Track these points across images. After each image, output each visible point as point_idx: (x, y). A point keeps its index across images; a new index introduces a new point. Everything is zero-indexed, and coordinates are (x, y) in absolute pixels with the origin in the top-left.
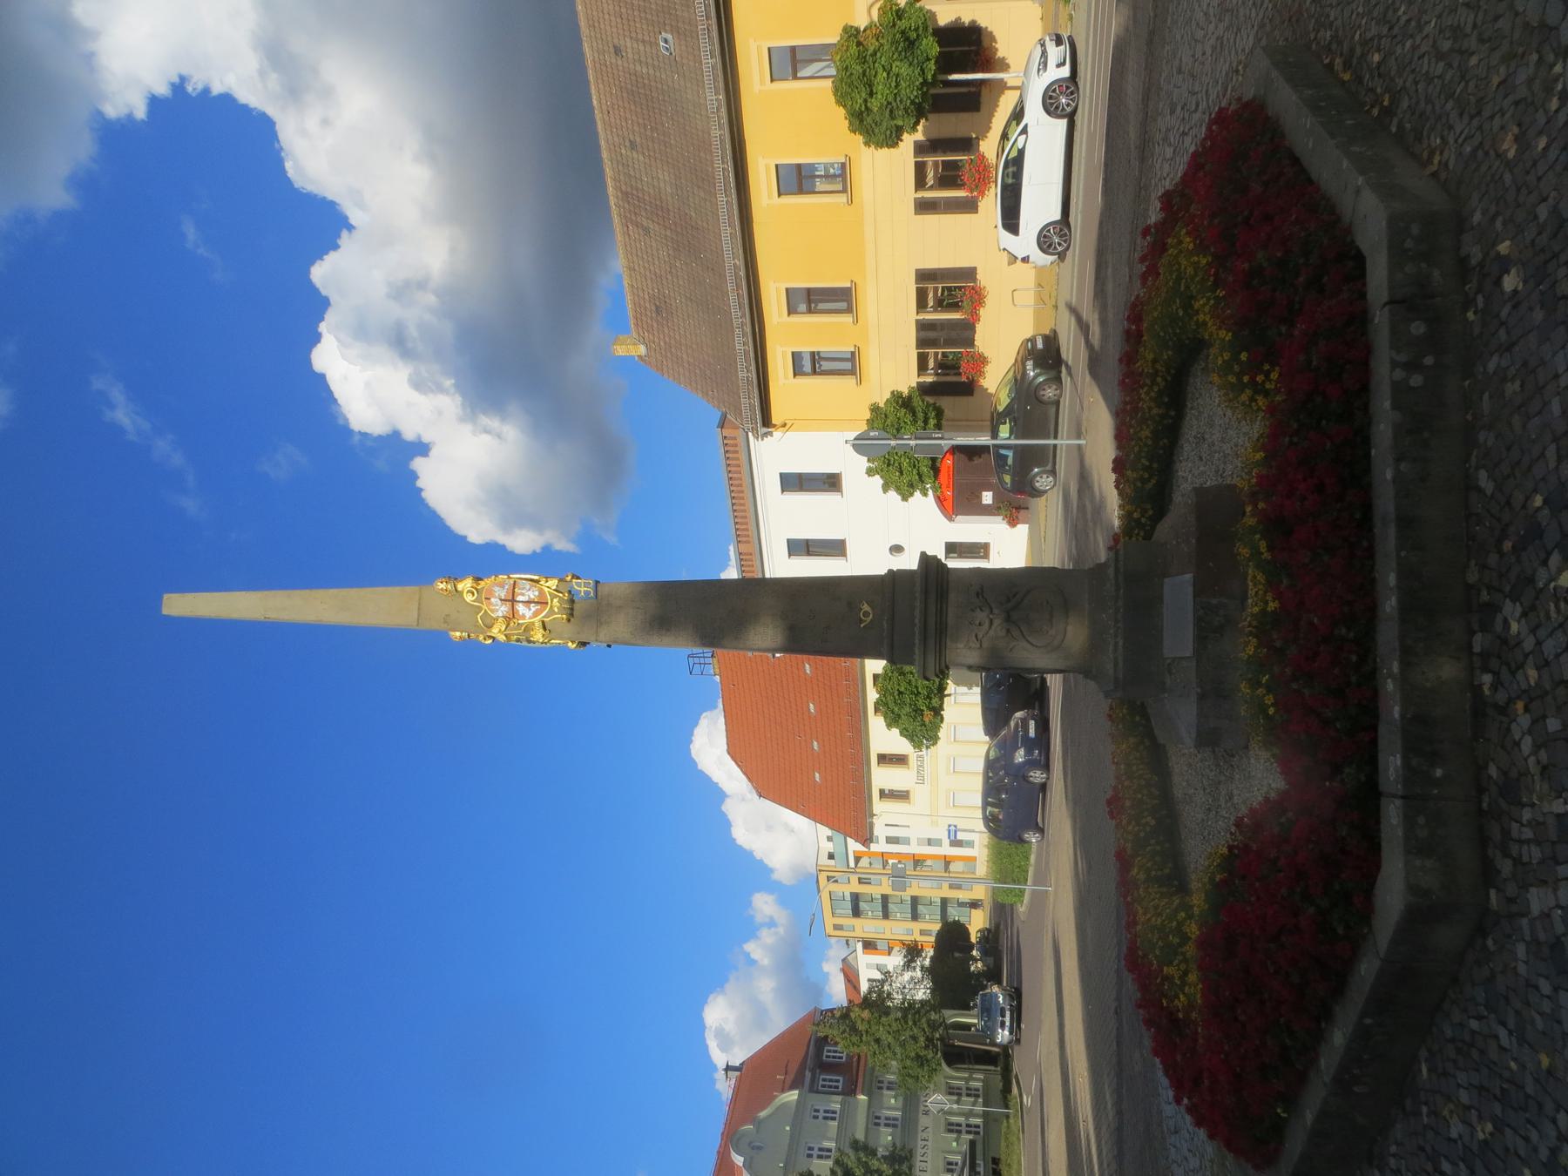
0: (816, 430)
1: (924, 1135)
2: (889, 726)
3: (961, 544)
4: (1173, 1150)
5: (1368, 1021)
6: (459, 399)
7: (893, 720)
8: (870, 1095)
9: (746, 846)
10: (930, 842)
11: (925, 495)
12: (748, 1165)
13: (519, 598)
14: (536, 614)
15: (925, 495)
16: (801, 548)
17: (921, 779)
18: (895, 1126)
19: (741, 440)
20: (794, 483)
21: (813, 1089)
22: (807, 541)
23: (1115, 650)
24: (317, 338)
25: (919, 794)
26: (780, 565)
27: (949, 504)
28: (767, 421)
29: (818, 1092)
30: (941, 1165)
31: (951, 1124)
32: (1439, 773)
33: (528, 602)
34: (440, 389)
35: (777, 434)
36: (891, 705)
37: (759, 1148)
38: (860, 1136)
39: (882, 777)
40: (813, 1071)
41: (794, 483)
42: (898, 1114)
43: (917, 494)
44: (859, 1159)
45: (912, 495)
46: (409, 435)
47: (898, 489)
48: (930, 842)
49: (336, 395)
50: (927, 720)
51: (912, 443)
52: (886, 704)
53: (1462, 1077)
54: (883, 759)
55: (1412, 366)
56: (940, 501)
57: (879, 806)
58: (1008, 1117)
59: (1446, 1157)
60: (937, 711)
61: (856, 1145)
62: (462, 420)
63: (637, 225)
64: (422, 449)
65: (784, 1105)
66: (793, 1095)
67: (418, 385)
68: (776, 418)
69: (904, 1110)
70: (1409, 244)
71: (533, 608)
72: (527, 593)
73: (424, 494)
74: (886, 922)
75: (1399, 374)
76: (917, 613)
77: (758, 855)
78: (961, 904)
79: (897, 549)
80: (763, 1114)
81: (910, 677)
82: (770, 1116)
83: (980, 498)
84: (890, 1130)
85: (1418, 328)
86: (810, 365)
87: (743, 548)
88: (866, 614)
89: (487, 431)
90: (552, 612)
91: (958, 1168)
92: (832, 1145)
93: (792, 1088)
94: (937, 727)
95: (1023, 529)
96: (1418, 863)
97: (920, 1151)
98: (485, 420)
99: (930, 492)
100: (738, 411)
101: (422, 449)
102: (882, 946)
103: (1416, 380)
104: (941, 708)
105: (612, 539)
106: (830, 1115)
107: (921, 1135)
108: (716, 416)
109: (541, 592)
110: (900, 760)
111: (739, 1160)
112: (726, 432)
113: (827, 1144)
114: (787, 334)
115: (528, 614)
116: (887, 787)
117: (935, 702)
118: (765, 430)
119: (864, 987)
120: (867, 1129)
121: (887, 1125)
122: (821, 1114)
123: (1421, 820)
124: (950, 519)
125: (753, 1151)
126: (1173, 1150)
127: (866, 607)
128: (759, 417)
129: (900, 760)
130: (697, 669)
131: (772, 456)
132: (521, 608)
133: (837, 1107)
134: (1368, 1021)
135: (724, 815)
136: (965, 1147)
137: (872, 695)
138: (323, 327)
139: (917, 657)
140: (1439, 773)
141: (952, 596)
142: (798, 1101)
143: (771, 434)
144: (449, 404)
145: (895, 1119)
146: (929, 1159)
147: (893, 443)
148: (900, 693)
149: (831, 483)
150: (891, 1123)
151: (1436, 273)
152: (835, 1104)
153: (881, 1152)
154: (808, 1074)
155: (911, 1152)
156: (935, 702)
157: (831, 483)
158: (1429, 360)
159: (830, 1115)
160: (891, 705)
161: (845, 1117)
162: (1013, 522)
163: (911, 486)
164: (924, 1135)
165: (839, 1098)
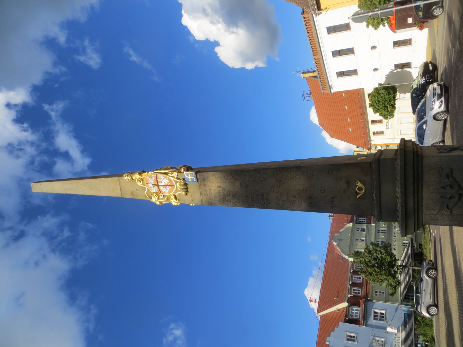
1: (395, 235)
2: (375, 113)
3: (399, 41)
6: (224, 24)
7: (376, 110)
8: (376, 223)
9: (331, 144)
11: (384, 26)
12: (338, 245)
13: (160, 184)
14: (170, 191)
15: (384, 26)
17: (388, 127)
18: (385, 233)
19: (311, 18)
20: (332, 30)
21: (357, 223)
22: (339, 51)
24: (182, 16)
27: (394, 26)
28: (319, 8)
29: (358, 223)
30: (401, 244)
33: (165, 186)
34: (219, 22)
35: (324, 12)
36: (375, 106)
37: (341, 240)
38: (373, 241)
39: (373, 128)
40: (356, 217)
41: (332, 30)
42: (386, 229)
43: (381, 26)
44: (373, 248)
45: (378, 27)
46: (212, 40)
47: (373, 26)
49: (192, 33)
50: (389, 109)
51: (379, 12)
52: (373, 106)
54: (373, 122)
56: (391, 27)
57: (372, 137)
58: (425, 233)
60: (393, 106)
61: (372, 244)
62: (226, 31)
64: (216, 44)
65: (348, 228)
66: (351, 225)
67: (212, 23)
68: (323, 7)
69: (388, 228)
71: (169, 188)
72: (164, 180)
73: (220, 58)
77: (334, 146)
80: (341, 230)
81: (382, 95)
82: (344, 231)
83: (407, 21)
84: (383, 234)
87: (316, 57)
88: (360, 189)
89: (233, 33)
90: (177, 190)
92: (364, 239)
93: (350, 222)
94: (393, 112)
95: (426, 30)
97: (393, 244)
98: (232, 29)
99: (386, 25)
100: (308, 6)
101: (216, 44)
104: (395, 104)
105: (277, 59)
106: (363, 230)
107: (393, 235)
108: (300, 10)
109: (170, 180)
110: (380, 121)
111: (335, 244)
112: (305, 16)
113: (362, 238)
115: (167, 191)
116: (375, 131)
117: (392, 103)
118: (319, 12)
120: (375, 234)
121: (382, 232)
122: (360, 230)
124: (395, 32)
125: (339, 241)
127: (359, 184)
128: (316, 7)
129: (380, 121)
130: (306, 99)
131: (322, 21)
132: (161, 188)
133: (365, 227)
135: (322, 136)
136: (410, 240)
137: (368, 101)
138: (183, 12)
141: (427, 178)
142: (352, 226)
143: (321, 13)
144: (221, 26)
145: (385, 230)
146: (397, 242)
147: (370, 14)
148: (379, 101)
150: (383, 232)
152: (364, 226)
153: (380, 245)
154: (355, 218)
155: (391, 244)
156: (392, 103)
159: (363, 230)
160: (375, 106)
161: (368, 232)
162: (421, 28)
163: (378, 23)
164: (395, 235)
165: (366, 225)
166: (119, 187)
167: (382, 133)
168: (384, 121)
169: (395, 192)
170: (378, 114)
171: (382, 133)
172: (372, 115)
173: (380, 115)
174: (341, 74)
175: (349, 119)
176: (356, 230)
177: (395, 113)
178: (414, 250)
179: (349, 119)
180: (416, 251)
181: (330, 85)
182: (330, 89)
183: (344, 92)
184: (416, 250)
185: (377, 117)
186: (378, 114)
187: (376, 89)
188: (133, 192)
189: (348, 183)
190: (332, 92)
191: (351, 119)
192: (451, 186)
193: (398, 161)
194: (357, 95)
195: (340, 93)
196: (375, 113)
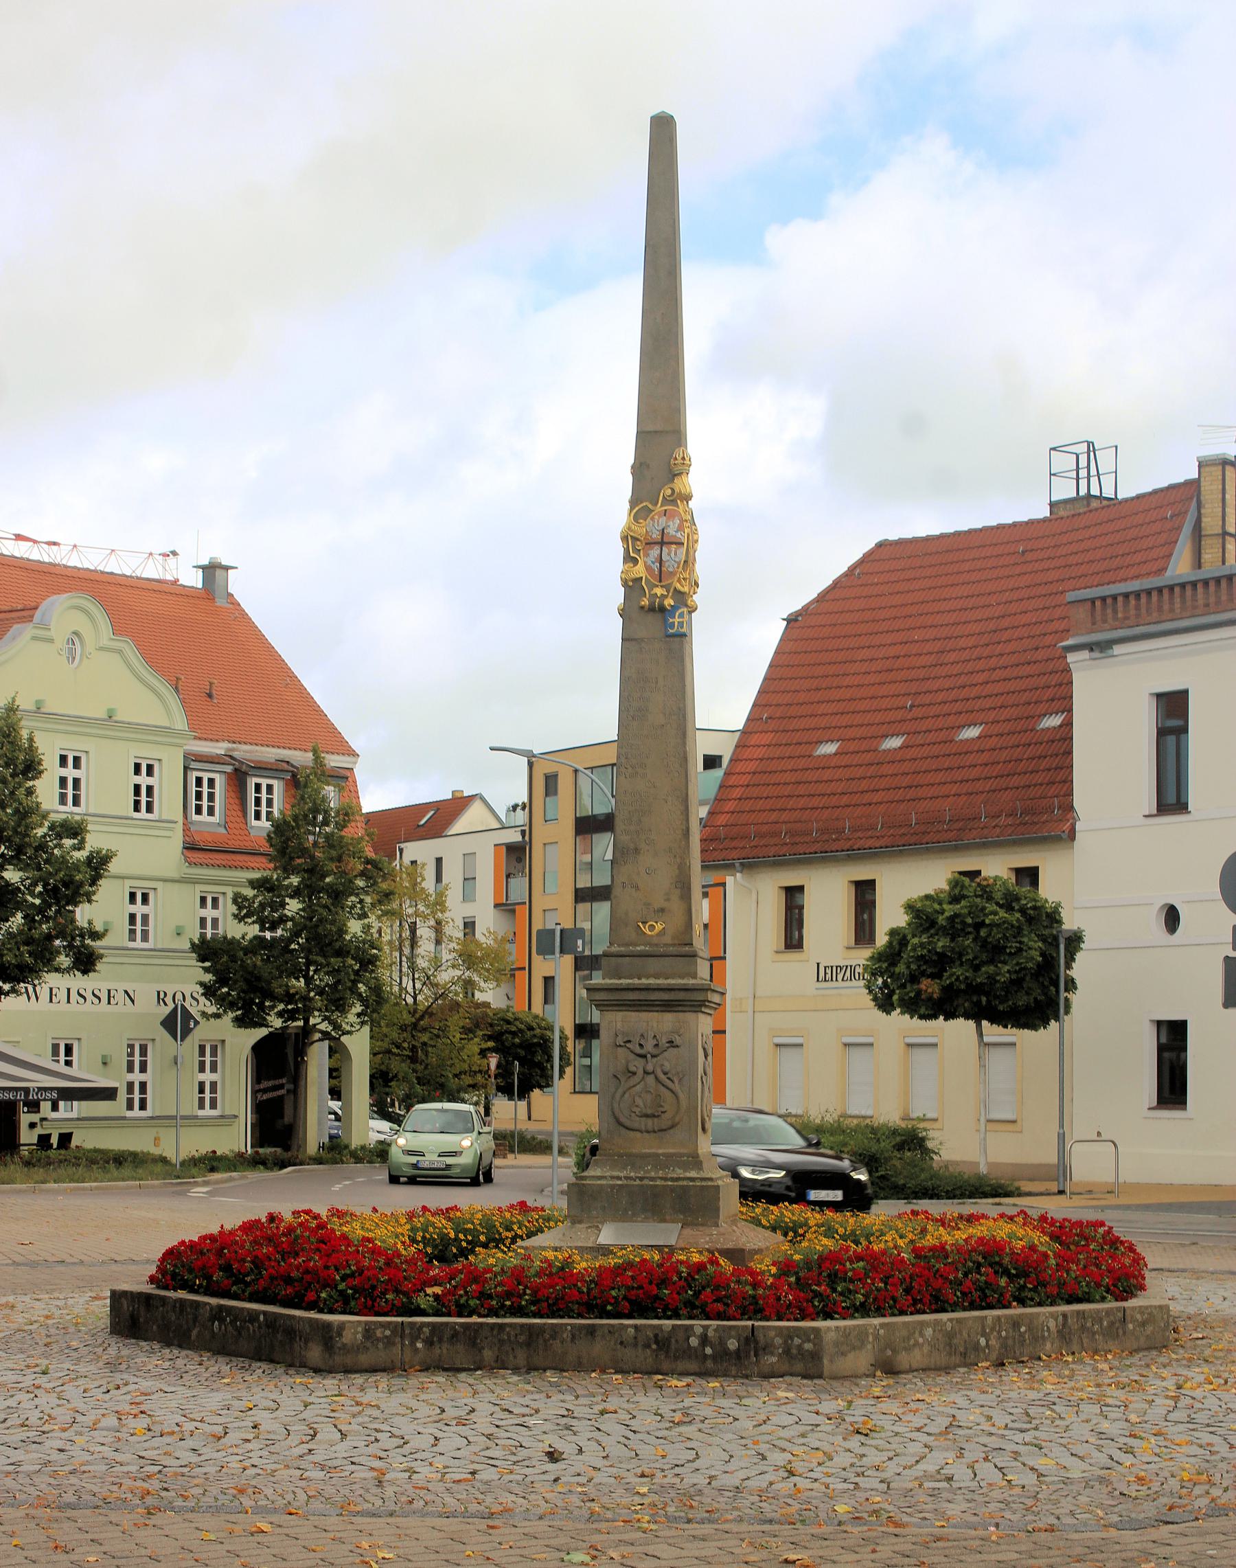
2: (910, 907)
5: (262, 1318)
7: (923, 915)
17: (827, 974)
23: (612, 1178)
25: (796, 972)
29: (186, 768)
31: (144, 1051)
32: (419, 1345)
55: (704, 1340)
70: (797, 1341)
74: (570, 897)
75: (699, 1331)
76: (652, 981)
85: (732, 1344)
88: (652, 928)
91: (61, 1067)
96: (360, 1329)
102: (518, 887)
103: (694, 1342)
110: (863, 931)
119: (416, 851)
123: (388, 1333)
132: (655, 552)
134: (262, 1318)
137: (996, 867)
139: (608, 981)
140: (419, 1345)
151: (774, 1359)
158: (708, 1351)
166: (659, 428)
167: (793, 940)
168: (862, 957)
169: (648, 977)
170: (901, 920)
171: (793, 940)
172: (905, 886)
173: (893, 933)
174: (1173, 709)
175: (894, 743)
176: (146, 753)
177: (899, 1021)
178: (34, 1106)
179: (894, 743)
180: (25, 1118)
181: (1117, 650)
182: (1090, 647)
183: (1068, 724)
184: (35, 1118)
185: (891, 916)
186: (901, 920)
187: (1054, 917)
188: (648, 466)
189: (662, 910)
190: (1071, 658)
191: (893, 757)
192: (657, 1045)
193: (692, 981)
194: (1039, 799)
195: (1061, 698)
196: (910, 907)
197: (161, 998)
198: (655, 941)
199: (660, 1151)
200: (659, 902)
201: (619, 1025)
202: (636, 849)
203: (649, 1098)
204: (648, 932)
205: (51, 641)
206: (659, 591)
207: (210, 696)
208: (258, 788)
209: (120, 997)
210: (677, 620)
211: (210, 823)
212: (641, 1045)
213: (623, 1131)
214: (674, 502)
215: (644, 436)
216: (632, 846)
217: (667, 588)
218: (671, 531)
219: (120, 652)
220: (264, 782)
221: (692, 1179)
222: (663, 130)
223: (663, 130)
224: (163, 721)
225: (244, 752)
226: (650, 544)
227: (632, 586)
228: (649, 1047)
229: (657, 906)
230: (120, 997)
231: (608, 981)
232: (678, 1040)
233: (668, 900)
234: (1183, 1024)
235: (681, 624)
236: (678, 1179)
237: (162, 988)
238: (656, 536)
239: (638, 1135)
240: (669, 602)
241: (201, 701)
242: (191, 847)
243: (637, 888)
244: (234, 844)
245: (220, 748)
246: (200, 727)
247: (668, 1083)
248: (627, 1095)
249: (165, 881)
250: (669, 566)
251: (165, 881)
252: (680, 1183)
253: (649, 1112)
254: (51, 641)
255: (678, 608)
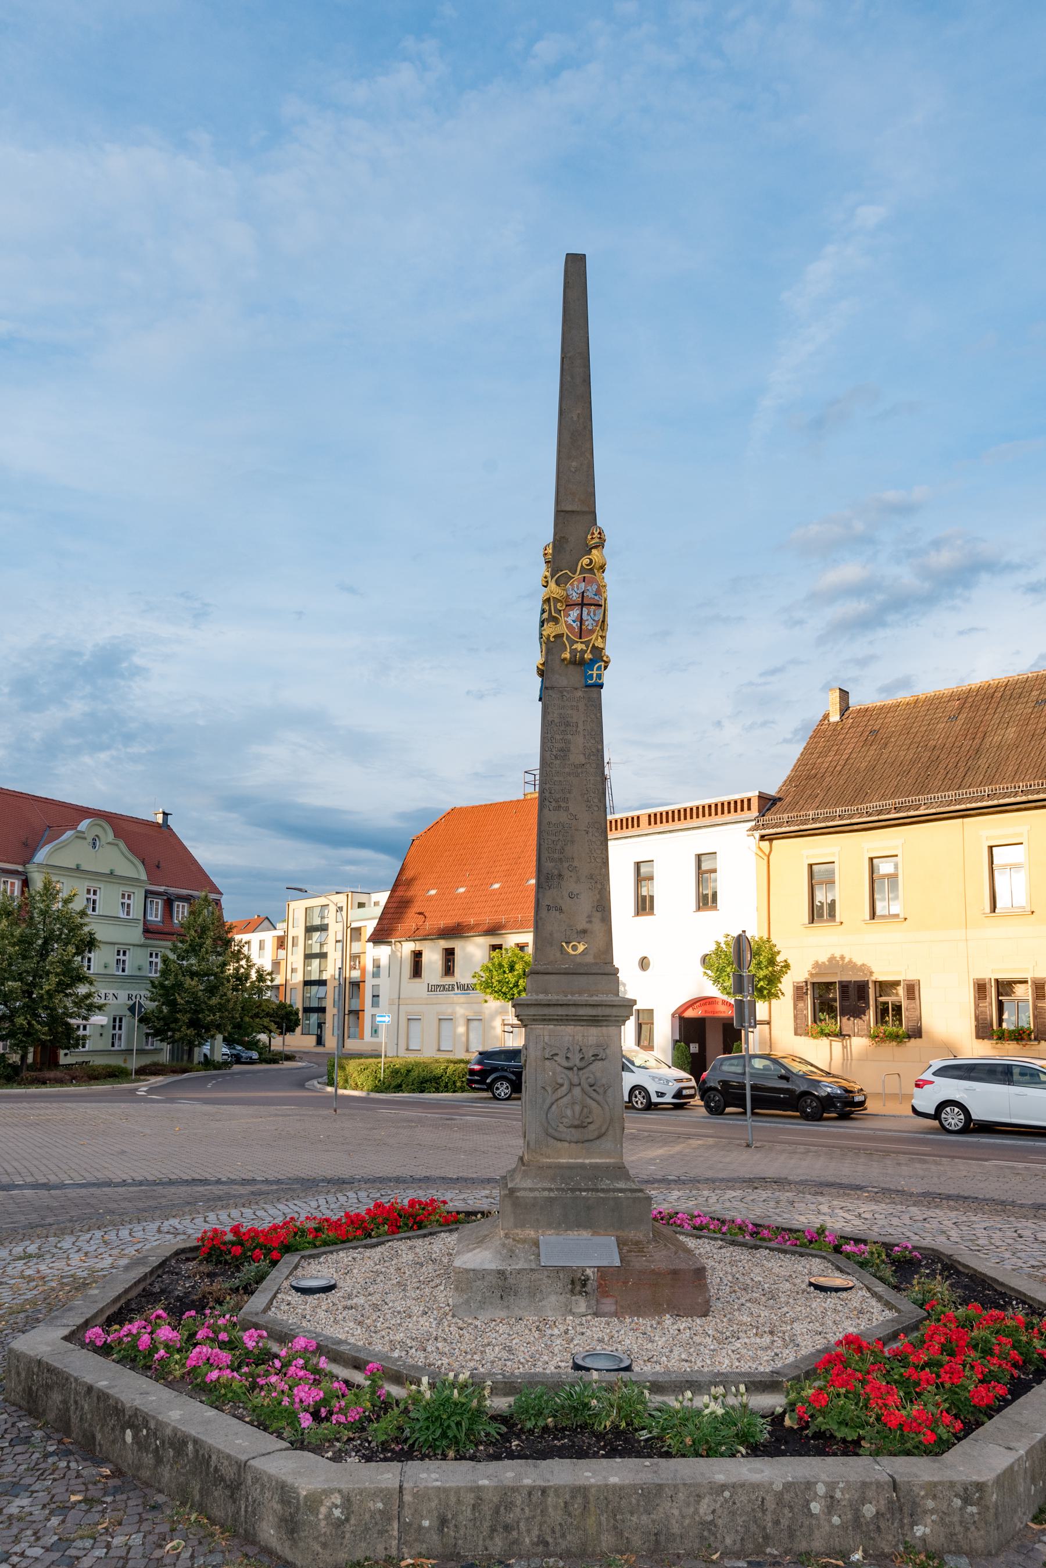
0: (756, 886)
4: (89, 1236)
10: (376, 996)
16: (642, 875)
17: (432, 988)
20: (703, 869)
26: (622, 854)
29: (146, 897)
31: (121, 1020)
37: (94, 845)
41: (703, 869)
48: (376, 996)
53: (137, 1539)
59: (63, 1521)
63: (960, 709)
78: (320, 1026)
79: (644, 964)
86: (817, 877)
88: (575, 948)
114: (847, 853)
116: (425, 958)
126: (89, 1236)
127: (581, 948)
131: (734, 843)
132: (574, 613)
149: (706, 901)
157: (706, 901)
166: (575, 508)
189: (584, 932)
197: (130, 997)
198: (578, 960)
199: (587, 1161)
200: (582, 924)
201: (546, 1039)
202: (560, 875)
203: (577, 1108)
204: (570, 950)
205: (85, 839)
206: (579, 647)
207: (158, 867)
208: (178, 906)
209: (111, 996)
210: (595, 673)
211: (156, 916)
212: (567, 1058)
213: (552, 1141)
214: (591, 571)
215: (561, 515)
216: (556, 872)
217: (587, 644)
218: (589, 594)
219: (117, 845)
220: (181, 904)
221: (621, 1190)
222: (575, 266)
223: (575, 266)
224: (133, 874)
225: (172, 890)
226: (570, 606)
227: (551, 646)
228: (576, 1060)
229: (580, 927)
230: (111, 996)
231: (535, 997)
232: (602, 1055)
233: (590, 922)
234: (921, 1037)
235: (599, 676)
236: (608, 1191)
237: (130, 992)
238: (575, 597)
239: (566, 1145)
240: (588, 656)
241: (154, 869)
242: (147, 931)
243: (561, 910)
244: (166, 930)
245: (161, 889)
246: (152, 880)
247: (594, 1095)
248: (554, 1107)
249: (134, 945)
250: (589, 624)
251: (134, 945)
252: (611, 1194)
253: (576, 1123)
254: (85, 839)
255: (597, 662)
